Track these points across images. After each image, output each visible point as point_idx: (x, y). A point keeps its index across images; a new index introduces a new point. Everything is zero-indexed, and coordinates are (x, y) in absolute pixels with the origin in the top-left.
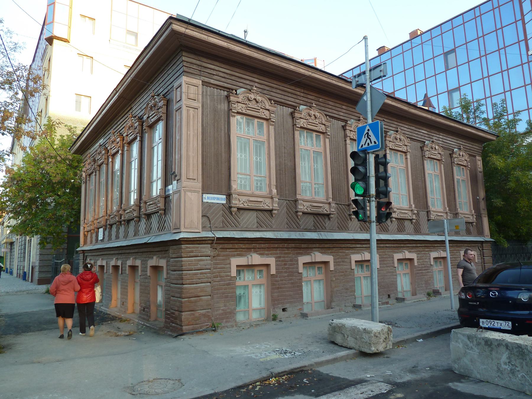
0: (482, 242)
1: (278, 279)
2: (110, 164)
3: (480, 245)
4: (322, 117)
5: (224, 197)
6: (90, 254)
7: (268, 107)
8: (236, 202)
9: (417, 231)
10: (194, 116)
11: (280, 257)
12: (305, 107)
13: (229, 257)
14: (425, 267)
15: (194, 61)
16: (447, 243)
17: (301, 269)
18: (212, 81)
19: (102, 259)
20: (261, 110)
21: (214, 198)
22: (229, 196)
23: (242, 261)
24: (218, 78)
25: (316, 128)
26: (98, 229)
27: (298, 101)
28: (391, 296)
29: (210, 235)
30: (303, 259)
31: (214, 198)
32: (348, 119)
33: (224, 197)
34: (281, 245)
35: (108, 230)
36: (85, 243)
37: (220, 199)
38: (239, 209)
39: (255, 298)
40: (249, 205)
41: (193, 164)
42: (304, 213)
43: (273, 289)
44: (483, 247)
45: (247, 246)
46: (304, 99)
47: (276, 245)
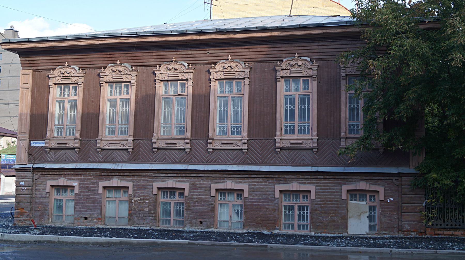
1: (81, 196)
3: (396, 178)
7: (309, 67)
13: (46, 179)
14: (265, 199)
17: (100, 191)
18: (39, 68)
21: (37, 143)
23: (107, 183)
31: (37, 143)
32: (216, 61)
34: (84, 173)
40: (223, 146)
45: (58, 173)
46: (110, 59)
47: (80, 173)
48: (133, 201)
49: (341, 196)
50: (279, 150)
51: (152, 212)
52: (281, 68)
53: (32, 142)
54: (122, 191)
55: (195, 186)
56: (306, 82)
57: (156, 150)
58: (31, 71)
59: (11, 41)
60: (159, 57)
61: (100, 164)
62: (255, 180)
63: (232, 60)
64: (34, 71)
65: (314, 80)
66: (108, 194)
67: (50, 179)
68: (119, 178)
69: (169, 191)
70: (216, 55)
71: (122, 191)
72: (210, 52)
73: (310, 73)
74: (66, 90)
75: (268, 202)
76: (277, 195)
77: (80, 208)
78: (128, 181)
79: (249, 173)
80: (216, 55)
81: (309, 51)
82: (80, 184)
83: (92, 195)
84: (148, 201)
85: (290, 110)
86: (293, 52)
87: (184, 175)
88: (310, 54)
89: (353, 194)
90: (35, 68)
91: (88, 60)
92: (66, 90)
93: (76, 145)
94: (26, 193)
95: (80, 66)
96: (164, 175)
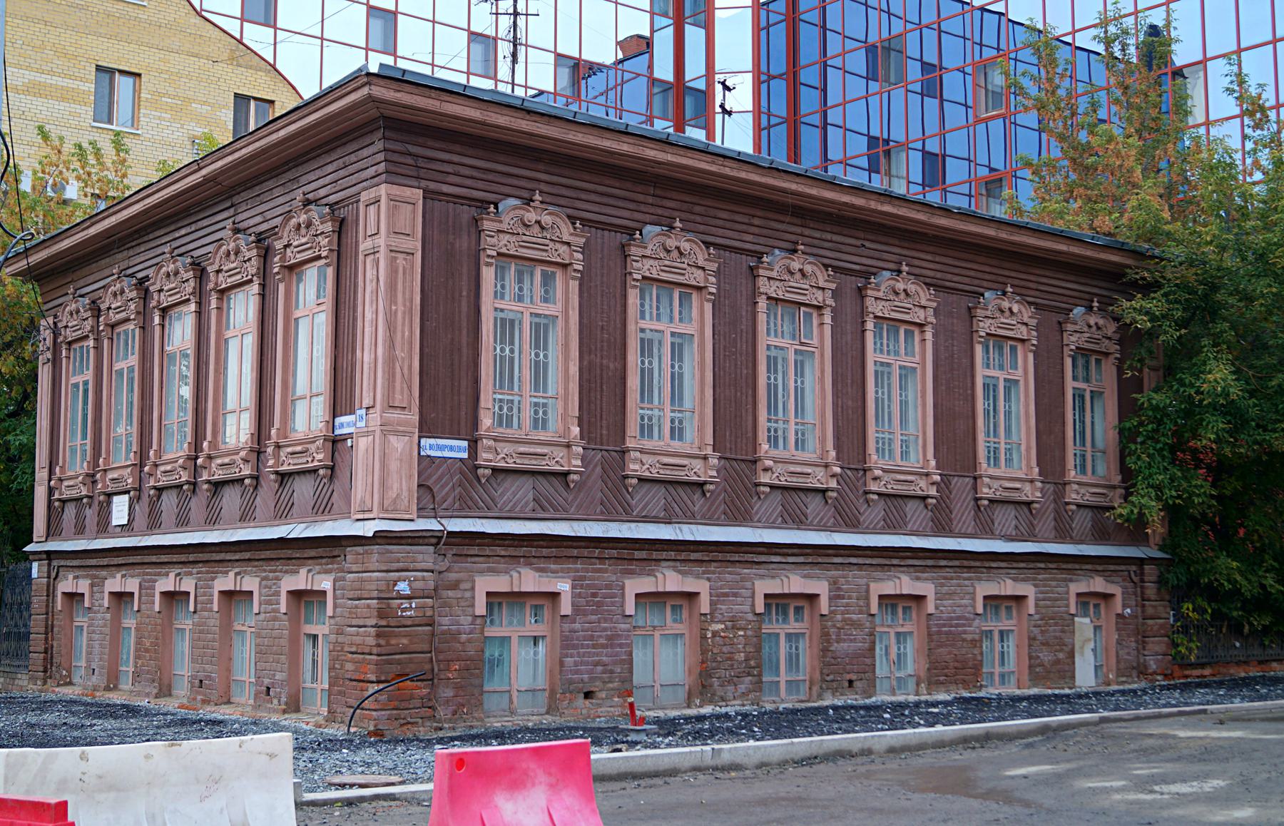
0: (1141, 562)
1: (577, 626)
3: (1134, 568)
5: (465, 444)
8: (484, 456)
9: (942, 528)
11: (583, 578)
14: (958, 618)
18: (446, 189)
20: (551, 245)
28: (855, 684)
29: (433, 525)
33: (465, 444)
34: (585, 552)
37: (455, 449)
38: (496, 470)
42: (641, 480)
44: (1142, 574)
45: (511, 551)
46: (652, 210)
48: (709, 635)
51: (752, 663)
52: (496, 226)
55: (839, 589)
57: (768, 489)
59: (630, 130)
60: (765, 232)
63: (544, 206)
64: (428, 194)
65: (574, 278)
66: (651, 618)
67: (481, 572)
68: (675, 569)
70: (877, 254)
72: (868, 244)
73: (1022, 332)
74: (665, 301)
75: (964, 625)
76: (630, 608)
77: (576, 664)
79: (727, 548)
80: (877, 254)
81: (1023, 283)
82: (573, 587)
83: (606, 621)
84: (741, 633)
86: (1001, 279)
90: (432, 186)
91: (593, 197)
92: (665, 301)
93: (574, 462)
94: (417, 621)
96: (778, 559)
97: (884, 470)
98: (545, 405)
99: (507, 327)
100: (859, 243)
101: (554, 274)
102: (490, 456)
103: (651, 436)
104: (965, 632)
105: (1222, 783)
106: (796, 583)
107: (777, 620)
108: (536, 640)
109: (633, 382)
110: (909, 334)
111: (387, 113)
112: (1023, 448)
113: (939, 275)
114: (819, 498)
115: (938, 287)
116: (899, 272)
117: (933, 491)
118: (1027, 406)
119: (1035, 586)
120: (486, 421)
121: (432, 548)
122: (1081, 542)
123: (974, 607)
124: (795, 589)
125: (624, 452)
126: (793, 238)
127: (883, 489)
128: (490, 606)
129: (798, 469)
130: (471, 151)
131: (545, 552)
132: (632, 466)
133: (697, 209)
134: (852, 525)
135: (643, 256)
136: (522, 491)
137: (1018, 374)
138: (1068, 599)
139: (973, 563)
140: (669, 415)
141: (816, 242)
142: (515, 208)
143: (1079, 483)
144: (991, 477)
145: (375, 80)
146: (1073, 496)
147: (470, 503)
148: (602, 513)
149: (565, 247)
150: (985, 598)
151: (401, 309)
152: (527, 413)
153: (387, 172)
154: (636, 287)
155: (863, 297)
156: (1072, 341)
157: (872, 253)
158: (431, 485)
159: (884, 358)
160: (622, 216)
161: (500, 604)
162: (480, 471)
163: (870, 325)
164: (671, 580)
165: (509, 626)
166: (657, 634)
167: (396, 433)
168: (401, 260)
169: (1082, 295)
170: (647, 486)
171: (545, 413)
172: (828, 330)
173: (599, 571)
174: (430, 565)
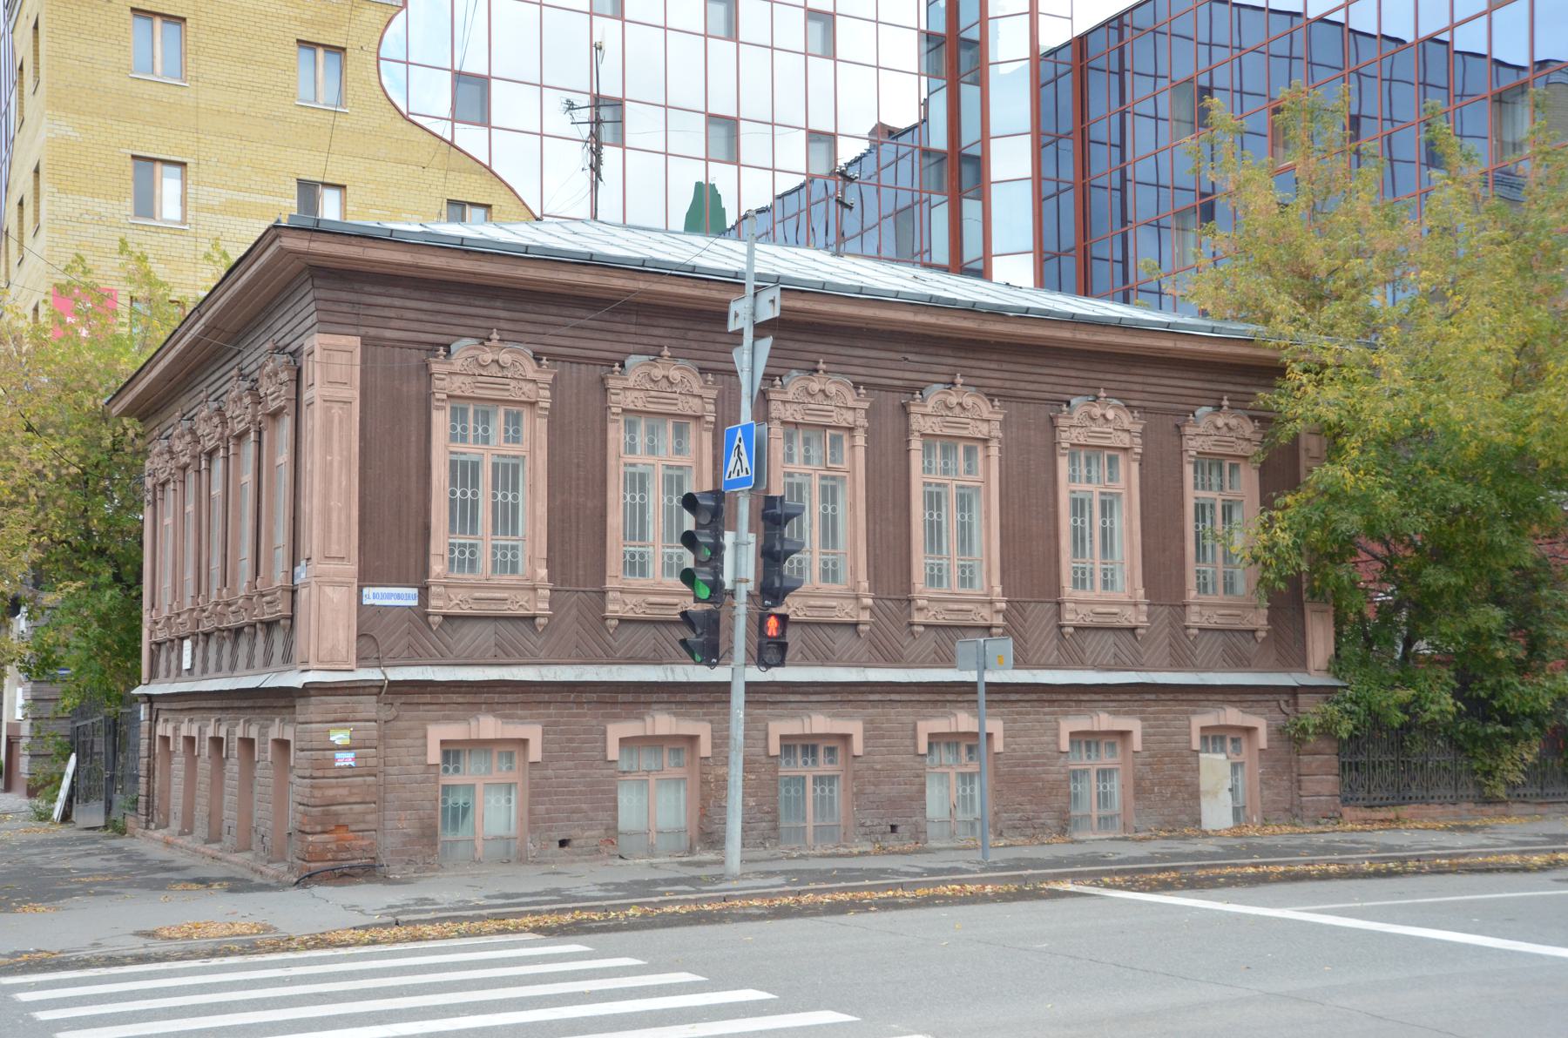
0: (1294, 691)
2: (204, 473)
3: (1286, 697)
4: (691, 377)
5: (415, 591)
6: (164, 706)
8: (436, 604)
10: (341, 421)
11: (556, 724)
12: (645, 358)
14: (1038, 757)
15: (344, 295)
16: (982, 689)
17: (613, 752)
18: (388, 334)
19: (191, 721)
20: (513, 383)
21: (389, 596)
22: (424, 591)
23: (632, 728)
24: (402, 324)
25: (672, 409)
26: (182, 639)
27: (618, 347)
28: (899, 829)
29: (374, 674)
30: (617, 730)
31: (389, 596)
33: (415, 591)
34: (559, 697)
35: (201, 644)
36: (153, 675)
37: (403, 597)
39: (496, 813)
41: (340, 525)
42: (622, 621)
43: (532, 795)
44: (1296, 704)
45: (469, 698)
46: (637, 339)
47: (546, 697)
49: (1190, 742)
50: (1071, 630)
53: (366, 591)
54: (495, 755)
56: (514, 420)
58: (355, 342)
61: (615, 668)
62: (1018, 708)
64: (367, 342)
65: (540, 416)
69: (799, 743)
71: (495, 755)
72: (910, 357)
73: (1125, 440)
76: (1065, 745)
77: (548, 811)
78: (698, 718)
81: (1123, 386)
82: (544, 733)
85: (464, 502)
86: (1091, 383)
87: (851, 697)
88: (1125, 395)
89: (1215, 737)
93: (540, 605)
94: (356, 771)
95: (537, 348)
97: (930, 600)
98: (513, 548)
99: (934, 500)
100: (899, 356)
101: (1116, 457)
102: (441, 603)
103: (1084, 587)
104: (1046, 773)
105: (771, 996)
106: (820, 723)
107: (806, 763)
108: (509, 786)
109: (615, 520)
110: (969, 452)
111: (312, 262)
112: (1126, 567)
113: (1008, 384)
114: (849, 633)
115: (1005, 398)
116: (953, 384)
117: (865, 616)
118: (1130, 521)
119: (1143, 720)
120: (437, 567)
121: (374, 698)
122: (1207, 669)
123: (1057, 744)
124: (1104, 727)
125: (604, 593)
126: (814, 356)
127: (932, 621)
128: (930, 745)
129: (819, 602)
130: (417, 294)
131: (510, 698)
132: (610, 607)
133: (691, 334)
134: (893, 659)
135: (625, 389)
136: (483, 635)
137: (1119, 486)
138: (1189, 734)
139: (1054, 697)
140: (660, 551)
141: (843, 359)
142: (469, 348)
143: (1201, 605)
144: (1076, 602)
145: (285, 232)
146: (1194, 618)
147: (421, 651)
148: (578, 656)
149: (531, 385)
150: (1072, 734)
151: (337, 458)
152: (955, 574)
153: (320, 321)
154: (443, 408)
155: (907, 414)
156: (1193, 446)
157: (918, 366)
158: (372, 633)
159: (936, 478)
160: (600, 347)
161: (1097, 744)
162: (608, 622)
163: (916, 444)
164: (663, 723)
165: (471, 772)
166: (652, 779)
167: (333, 584)
168: (336, 410)
169: (1207, 393)
170: (632, 628)
171: (514, 556)
172: (860, 454)
173: (577, 715)
174: (373, 715)
